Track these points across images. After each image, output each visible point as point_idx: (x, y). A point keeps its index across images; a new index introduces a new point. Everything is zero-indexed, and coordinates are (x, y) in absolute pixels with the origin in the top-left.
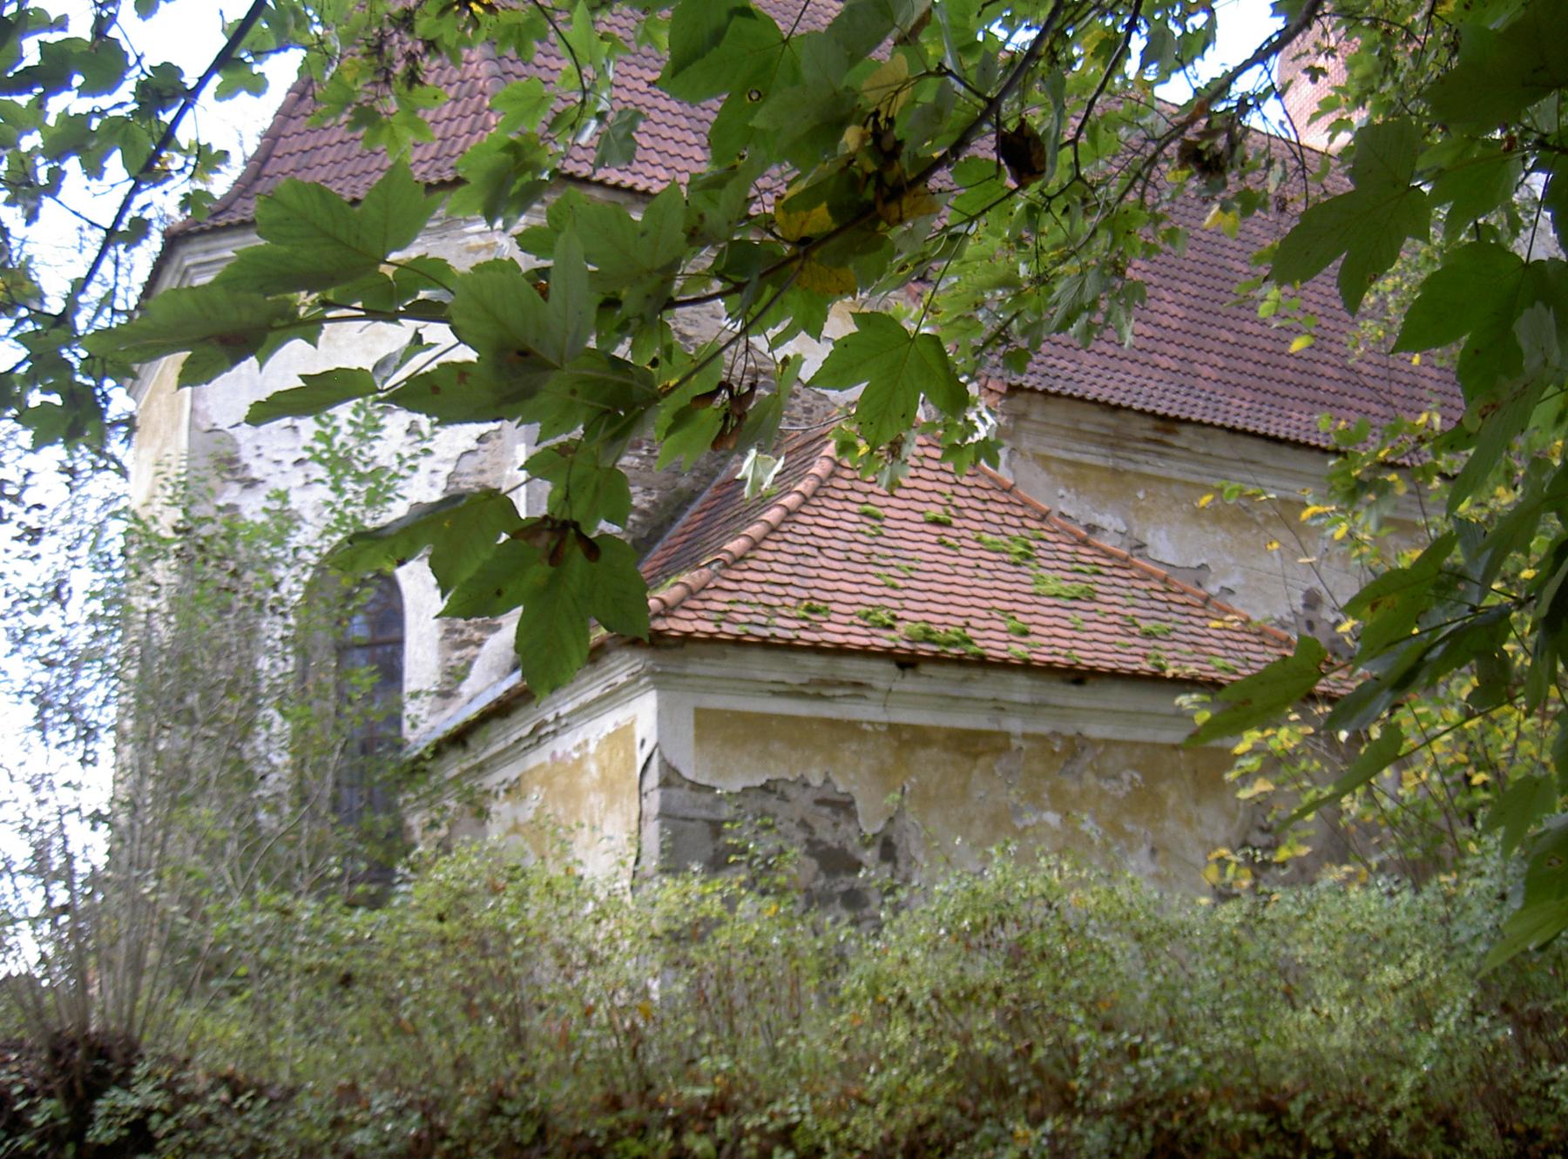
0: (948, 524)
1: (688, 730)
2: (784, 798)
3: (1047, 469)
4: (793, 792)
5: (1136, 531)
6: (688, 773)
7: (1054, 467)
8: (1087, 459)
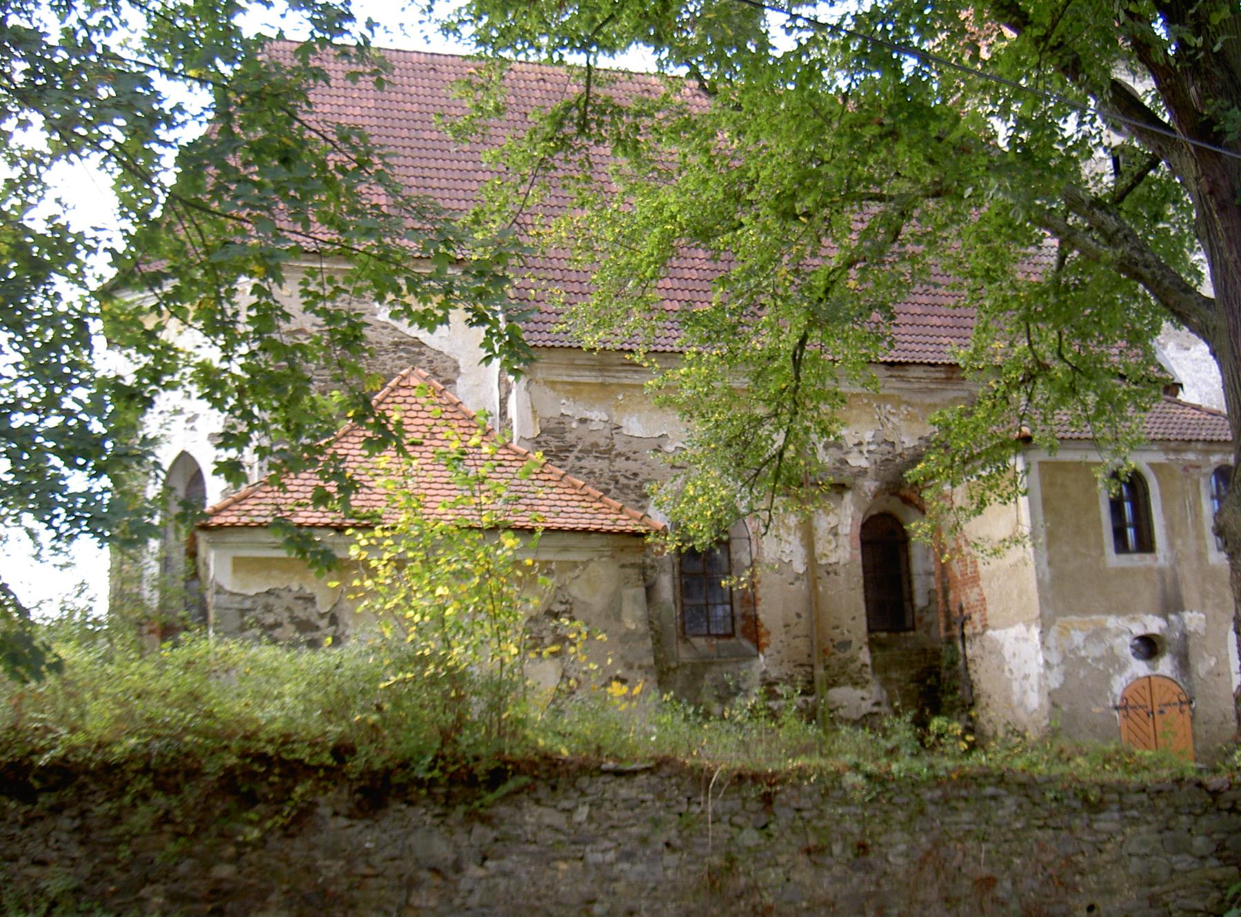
0: (421, 444)
1: (229, 567)
2: (278, 597)
3: (553, 389)
4: (283, 594)
5: (615, 419)
6: (228, 587)
7: (559, 387)
8: (582, 380)
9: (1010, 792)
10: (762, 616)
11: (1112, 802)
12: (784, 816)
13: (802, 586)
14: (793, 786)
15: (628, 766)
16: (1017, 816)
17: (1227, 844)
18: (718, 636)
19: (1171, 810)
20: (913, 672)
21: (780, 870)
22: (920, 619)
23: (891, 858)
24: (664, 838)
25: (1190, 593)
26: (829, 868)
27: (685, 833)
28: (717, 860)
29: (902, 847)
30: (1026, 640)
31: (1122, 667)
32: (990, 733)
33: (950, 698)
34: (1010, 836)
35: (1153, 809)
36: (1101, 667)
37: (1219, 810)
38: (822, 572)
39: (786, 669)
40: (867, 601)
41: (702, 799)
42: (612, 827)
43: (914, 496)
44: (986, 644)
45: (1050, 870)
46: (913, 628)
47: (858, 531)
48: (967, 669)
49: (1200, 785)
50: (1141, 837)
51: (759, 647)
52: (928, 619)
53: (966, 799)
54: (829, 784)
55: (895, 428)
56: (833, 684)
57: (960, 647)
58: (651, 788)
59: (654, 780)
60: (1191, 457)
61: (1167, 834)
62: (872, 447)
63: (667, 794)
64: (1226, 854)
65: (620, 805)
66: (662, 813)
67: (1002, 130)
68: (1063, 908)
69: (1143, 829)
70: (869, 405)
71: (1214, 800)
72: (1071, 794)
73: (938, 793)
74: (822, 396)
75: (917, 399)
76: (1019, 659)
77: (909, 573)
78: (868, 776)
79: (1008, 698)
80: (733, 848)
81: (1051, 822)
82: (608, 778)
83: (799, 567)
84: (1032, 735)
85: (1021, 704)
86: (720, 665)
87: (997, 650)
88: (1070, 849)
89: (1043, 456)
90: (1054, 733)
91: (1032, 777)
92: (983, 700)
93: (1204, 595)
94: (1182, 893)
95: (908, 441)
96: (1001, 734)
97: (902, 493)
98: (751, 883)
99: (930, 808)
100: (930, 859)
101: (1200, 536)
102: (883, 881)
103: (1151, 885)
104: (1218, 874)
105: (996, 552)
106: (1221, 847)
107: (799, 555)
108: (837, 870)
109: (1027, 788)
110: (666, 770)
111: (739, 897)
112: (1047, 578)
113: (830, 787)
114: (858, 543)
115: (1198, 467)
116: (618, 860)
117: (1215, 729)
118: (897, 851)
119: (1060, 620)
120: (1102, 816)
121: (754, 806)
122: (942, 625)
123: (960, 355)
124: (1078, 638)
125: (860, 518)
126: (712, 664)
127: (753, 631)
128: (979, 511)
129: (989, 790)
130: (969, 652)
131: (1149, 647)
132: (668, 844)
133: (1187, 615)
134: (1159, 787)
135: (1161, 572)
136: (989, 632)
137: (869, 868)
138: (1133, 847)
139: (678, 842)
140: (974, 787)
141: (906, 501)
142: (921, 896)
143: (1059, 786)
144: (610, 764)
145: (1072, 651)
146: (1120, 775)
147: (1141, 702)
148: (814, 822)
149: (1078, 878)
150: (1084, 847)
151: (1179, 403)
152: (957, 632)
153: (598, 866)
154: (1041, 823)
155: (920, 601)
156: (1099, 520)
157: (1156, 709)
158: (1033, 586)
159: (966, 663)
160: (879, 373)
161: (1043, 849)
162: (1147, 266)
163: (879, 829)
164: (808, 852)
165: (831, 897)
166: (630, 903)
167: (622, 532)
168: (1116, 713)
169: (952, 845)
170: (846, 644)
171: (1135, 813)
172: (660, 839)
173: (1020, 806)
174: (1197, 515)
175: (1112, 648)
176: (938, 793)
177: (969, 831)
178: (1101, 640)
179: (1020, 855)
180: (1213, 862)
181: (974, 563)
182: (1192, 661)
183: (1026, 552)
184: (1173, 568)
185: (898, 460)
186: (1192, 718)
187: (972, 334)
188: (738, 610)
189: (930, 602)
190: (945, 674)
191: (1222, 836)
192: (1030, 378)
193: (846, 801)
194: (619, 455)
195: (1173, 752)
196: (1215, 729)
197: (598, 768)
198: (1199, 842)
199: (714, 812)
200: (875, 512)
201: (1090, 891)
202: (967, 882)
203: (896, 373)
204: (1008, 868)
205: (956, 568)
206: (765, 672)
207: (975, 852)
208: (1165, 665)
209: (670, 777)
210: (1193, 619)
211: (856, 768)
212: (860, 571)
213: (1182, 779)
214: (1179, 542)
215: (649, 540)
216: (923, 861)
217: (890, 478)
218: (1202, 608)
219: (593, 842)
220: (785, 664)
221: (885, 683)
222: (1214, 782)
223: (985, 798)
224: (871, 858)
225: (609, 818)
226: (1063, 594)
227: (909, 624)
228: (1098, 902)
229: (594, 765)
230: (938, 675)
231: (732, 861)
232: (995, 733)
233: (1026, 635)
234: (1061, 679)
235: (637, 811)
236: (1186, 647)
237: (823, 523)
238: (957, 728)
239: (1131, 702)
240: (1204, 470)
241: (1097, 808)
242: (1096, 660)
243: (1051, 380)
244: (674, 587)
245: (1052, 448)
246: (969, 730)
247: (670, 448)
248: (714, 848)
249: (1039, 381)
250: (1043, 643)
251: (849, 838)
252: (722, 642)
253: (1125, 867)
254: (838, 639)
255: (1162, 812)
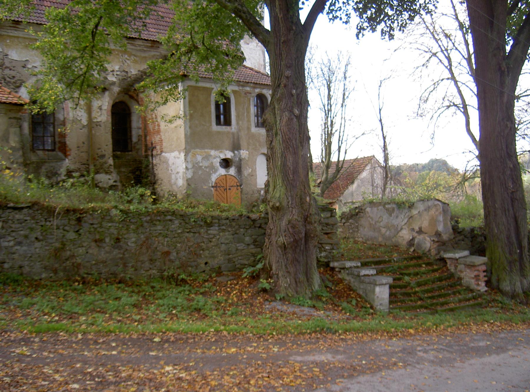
9: (177, 219)
10: (68, 143)
11: (216, 223)
12: (86, 227)
13: (85, 130)
14: (91, 214)
15: (20, 206)
16: (179, 228)
17: (258, 240)
18: (48, 150)
19: (238, 227)
20: (130, 169)
21: (84, 249)
22: (135, 147)
23: (129, 244)
24: (35, 236)
25: (243, 143)
26: (104, 248)
27: (44, 234)
28: (58, 245)
29: (134, 239)
30: (178, 158)
31: (216, 171)
32: (162, 195)
33: (146, 180)
34: (176, 235)
35: (231, 226)
36: (208, 170)
37: (255, 227)
38: (94, 125)
39: (77, 166)
40: (113, 138)
41: (52, 219)
42: (12, 231)
43: (135, 95)
44: (162, 159)
45: (191, 249)
46: (131, 151)
47: (110, 108)
48: (153, 169)
49: (248, 217)
50: (227, 236)
51: (66, 156)
52: (138, 147)
53: (160, 221)
54: (105, 214)
55: (129, 65)
56: (97, 172)
57: (151, 159)
58: (29, 215)
59: (31, 211)
60: (248, 89)
61: (236, 235)
62: (118, 73)
63: (36, 217)
64: (257, 243)
65: (16, 222)
66: (34, 225)
68: (196, 263)
69: (227, 233)
70: (118, 54)
71: (254, 223)
72: (200, 219)
73: (149, 218)
74: (104, 50)
75: (139, 54)
76: (175, 165)
77: (130, 127)
78: (121, 211)
79: (170, 181)
80: (65, 240)
81: (192, 230)
82: (11, 211)
83: (85, 122)
84: (180, 196)
85: (175, 184)
86: (49, 163)
87: (166, 162)
88: (199, 241)
89: (192, 83)
90: (188, 196)
91: (185, 213)
92: (159, 182)
93: (249, 144)
94: (240, 258)
95: (134, 71)
96: (166, 196)
97: (130, 93)
98: (72, 254)
99: (146, 224)
100: (145, 244)
101: (249, 121)
102: (126, 253)
103: (229, 255)
104: (253, 251)
105: (170, 121)
106: (255, 241)
107: (85, 117)
108: (107, 248)
109: (183, 217)
110: (36, 207)
111: (67, 260)
112: (189, 134)
113: (106, 215)
114: (110, 113)
115: (250, 93)
116: (15, 245)
117: (249, 197)
118: (132, 240)
119: (192, 151)
120: (212, 228)
121: (73, 222)
122: (144, 150)
123: (162, 38)
124: (199, 158)
125: (111, 103)
126: (45, 162)
127: (63, 148)
128: (165, 103)
129: (169, 217)
130: (154, 162)
131: (226, 163)
132: (36, 238)
133: (242, 152)
134: (233, 218)
135: (233, 134)
136: (163, 154)
137: (120, 248)
138: (223, 240)
139: (41, 238)
140: (163, 216)
141: (131, 97)
142: (141, 259)
143: (196, 216)
144: (12, 205)
145: (197, 163)
146: (217, 213)
147: (223, 185)
148: (98, 229)
149: (201, 252)
150: (205, 240)
151: (244, 66)
152: (150, 153)
153: (6, 248)
154: (188, 230)
155: (134, 139)
156: (210, 111)
157: (228, 188)
158: (183, 136)
159: (153, 167)
160: (125, 41)
161: (188, 241)
162: (244, 13)
163: (125, 232)
164: (96, 241)
165: (105, 259)
166: (20, 263)
167: (10, 103)
168: (212, 189)
169: (154, 238)
170: (103, 156)
171: (224, 227)
172: (33, 236)
173: (180, 224)
174: (248, 112)
175: (212, 163)
176: (149, 218)
177: (161, 233)
178: (208, 160)
179: (180, 243)
180: (252, 246)
181: (159, 125)
182: (242, 170)
183: (180, 122)
184: (238, 133)
185: (129, 79)
186: (241, 192)
187: (168, 29)
188: (57, 139)
189: (139, 140)
190: (144, 170)
191: (256, 237)
192: (189, 51)
193: (111, 221)
194: (6, 68)
195: (235, 205)
196: (249, 197)
197: (6, 206)
198: (247, 239)
199: (57, 225)
200: (117, 101)
201: (206, 257)
202: (159, 253)
203: (130, 42)
204: (175, 248)
205: (151, 127)
207: (162, 241)
208: (232, 171)
209: (37, 210)
210: (244, 153)
211: (116, 207)
212: (110, 125)
213: (242, 215)
214: (240, 123)
215: (26, 107)
216: (142, 245)
217: (125, 87)
218: (248, 149)
219: (4, 238)
221: (119, 173)
222: (254, 216)
223: (167, 220)
224: (121, 244)
225: (11, 227)
226: (195, 140)
227: (130, 149)
228: (209, 261)
229: (5, 205)
230: (141, 170)
231: (64, 245)
232: (164, 195)
233: (178, 156)
234: (192, 174)
235: (23, 224)
236: (241, 164)
237: (96, 104)
238: (148, 192)
239: (218, 185)
240: (253, 95)
241: (209, 225)
242: (205, 167)
243: (198, 53)
244: (30, 128)
245: (197, 81)
246: (154, 193)
247: (30, 66)
248: (57, 240)
249: (194, 53)
250: (185, 159)
251: (112, 236)
252: (50, 153)
253: (219, 248)
254: (100, 154)
255: (234, 227)
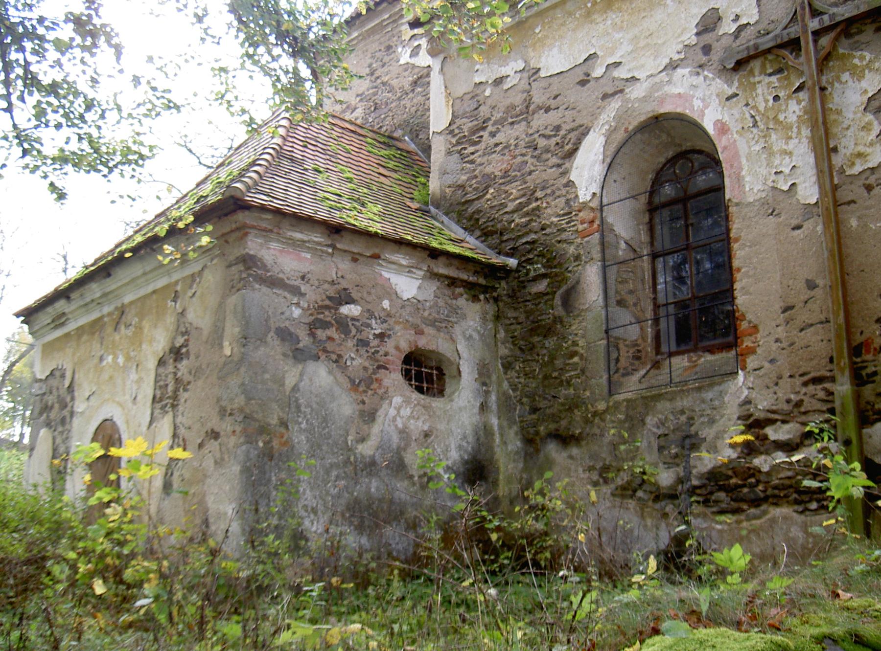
13: (816, 227)
38: (856, 191)
39: (787, 391)
67: (612, 431)
83: (809, 192)
206: (748, 402)
220: (785, 383)
